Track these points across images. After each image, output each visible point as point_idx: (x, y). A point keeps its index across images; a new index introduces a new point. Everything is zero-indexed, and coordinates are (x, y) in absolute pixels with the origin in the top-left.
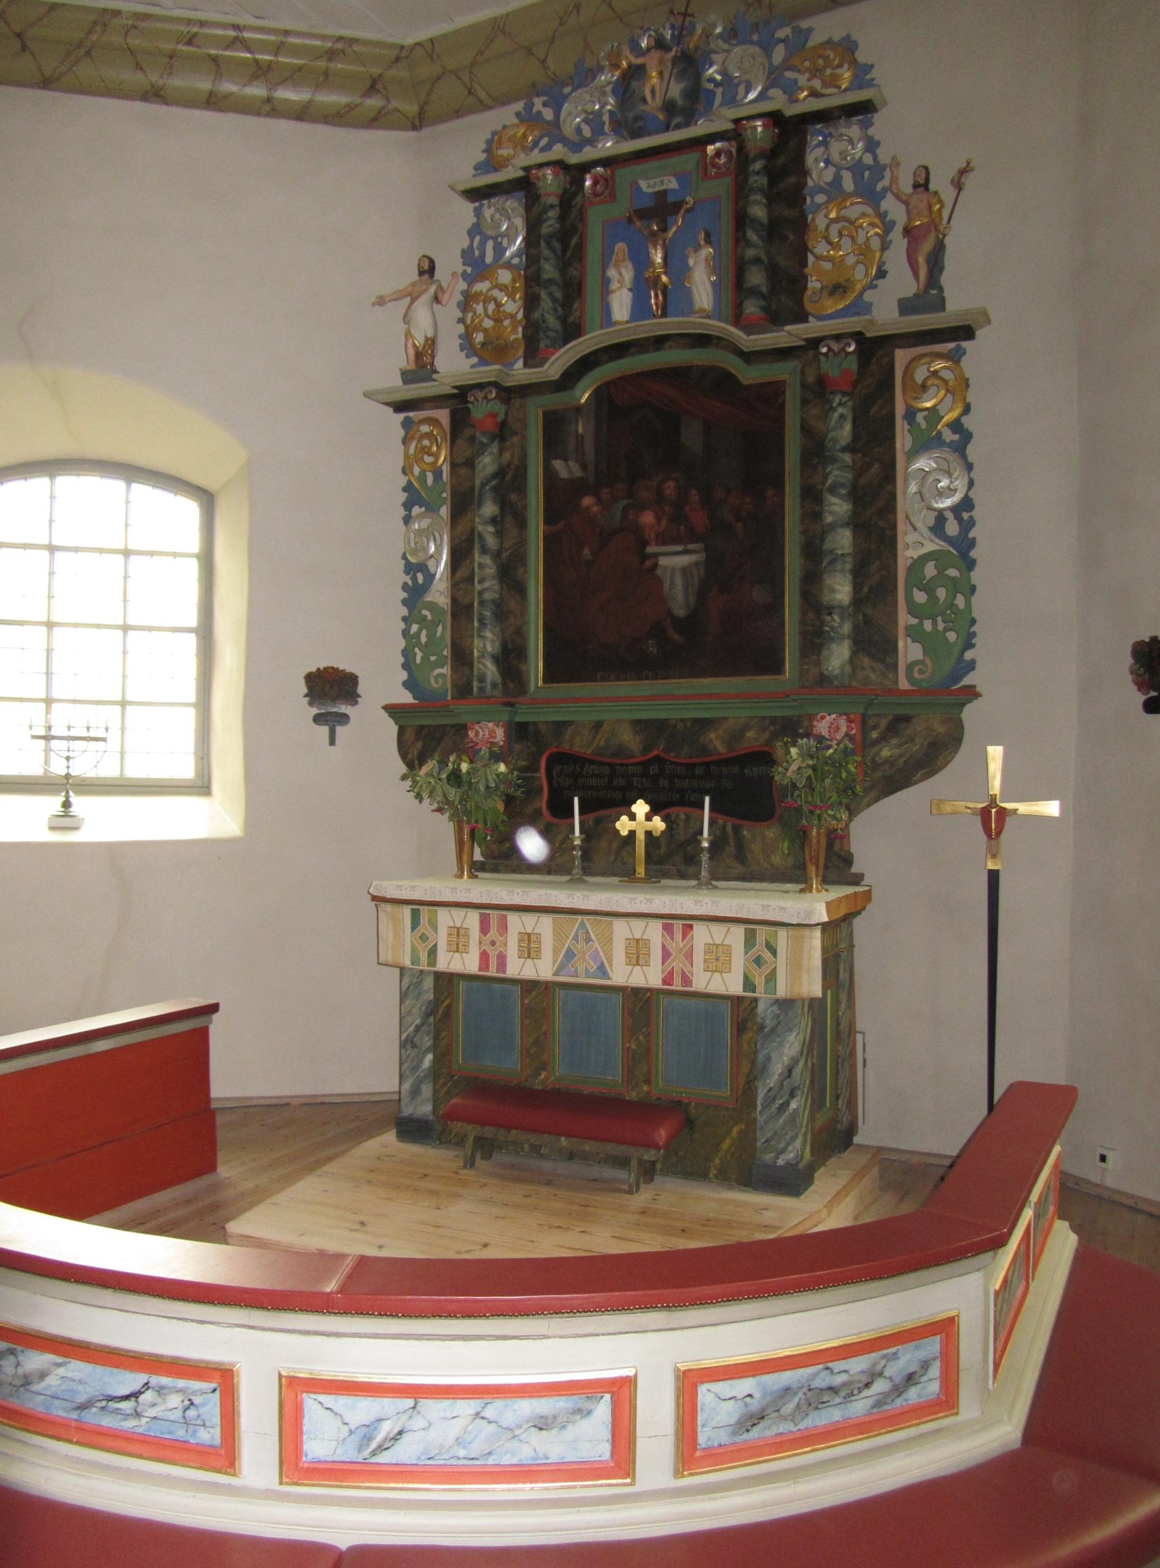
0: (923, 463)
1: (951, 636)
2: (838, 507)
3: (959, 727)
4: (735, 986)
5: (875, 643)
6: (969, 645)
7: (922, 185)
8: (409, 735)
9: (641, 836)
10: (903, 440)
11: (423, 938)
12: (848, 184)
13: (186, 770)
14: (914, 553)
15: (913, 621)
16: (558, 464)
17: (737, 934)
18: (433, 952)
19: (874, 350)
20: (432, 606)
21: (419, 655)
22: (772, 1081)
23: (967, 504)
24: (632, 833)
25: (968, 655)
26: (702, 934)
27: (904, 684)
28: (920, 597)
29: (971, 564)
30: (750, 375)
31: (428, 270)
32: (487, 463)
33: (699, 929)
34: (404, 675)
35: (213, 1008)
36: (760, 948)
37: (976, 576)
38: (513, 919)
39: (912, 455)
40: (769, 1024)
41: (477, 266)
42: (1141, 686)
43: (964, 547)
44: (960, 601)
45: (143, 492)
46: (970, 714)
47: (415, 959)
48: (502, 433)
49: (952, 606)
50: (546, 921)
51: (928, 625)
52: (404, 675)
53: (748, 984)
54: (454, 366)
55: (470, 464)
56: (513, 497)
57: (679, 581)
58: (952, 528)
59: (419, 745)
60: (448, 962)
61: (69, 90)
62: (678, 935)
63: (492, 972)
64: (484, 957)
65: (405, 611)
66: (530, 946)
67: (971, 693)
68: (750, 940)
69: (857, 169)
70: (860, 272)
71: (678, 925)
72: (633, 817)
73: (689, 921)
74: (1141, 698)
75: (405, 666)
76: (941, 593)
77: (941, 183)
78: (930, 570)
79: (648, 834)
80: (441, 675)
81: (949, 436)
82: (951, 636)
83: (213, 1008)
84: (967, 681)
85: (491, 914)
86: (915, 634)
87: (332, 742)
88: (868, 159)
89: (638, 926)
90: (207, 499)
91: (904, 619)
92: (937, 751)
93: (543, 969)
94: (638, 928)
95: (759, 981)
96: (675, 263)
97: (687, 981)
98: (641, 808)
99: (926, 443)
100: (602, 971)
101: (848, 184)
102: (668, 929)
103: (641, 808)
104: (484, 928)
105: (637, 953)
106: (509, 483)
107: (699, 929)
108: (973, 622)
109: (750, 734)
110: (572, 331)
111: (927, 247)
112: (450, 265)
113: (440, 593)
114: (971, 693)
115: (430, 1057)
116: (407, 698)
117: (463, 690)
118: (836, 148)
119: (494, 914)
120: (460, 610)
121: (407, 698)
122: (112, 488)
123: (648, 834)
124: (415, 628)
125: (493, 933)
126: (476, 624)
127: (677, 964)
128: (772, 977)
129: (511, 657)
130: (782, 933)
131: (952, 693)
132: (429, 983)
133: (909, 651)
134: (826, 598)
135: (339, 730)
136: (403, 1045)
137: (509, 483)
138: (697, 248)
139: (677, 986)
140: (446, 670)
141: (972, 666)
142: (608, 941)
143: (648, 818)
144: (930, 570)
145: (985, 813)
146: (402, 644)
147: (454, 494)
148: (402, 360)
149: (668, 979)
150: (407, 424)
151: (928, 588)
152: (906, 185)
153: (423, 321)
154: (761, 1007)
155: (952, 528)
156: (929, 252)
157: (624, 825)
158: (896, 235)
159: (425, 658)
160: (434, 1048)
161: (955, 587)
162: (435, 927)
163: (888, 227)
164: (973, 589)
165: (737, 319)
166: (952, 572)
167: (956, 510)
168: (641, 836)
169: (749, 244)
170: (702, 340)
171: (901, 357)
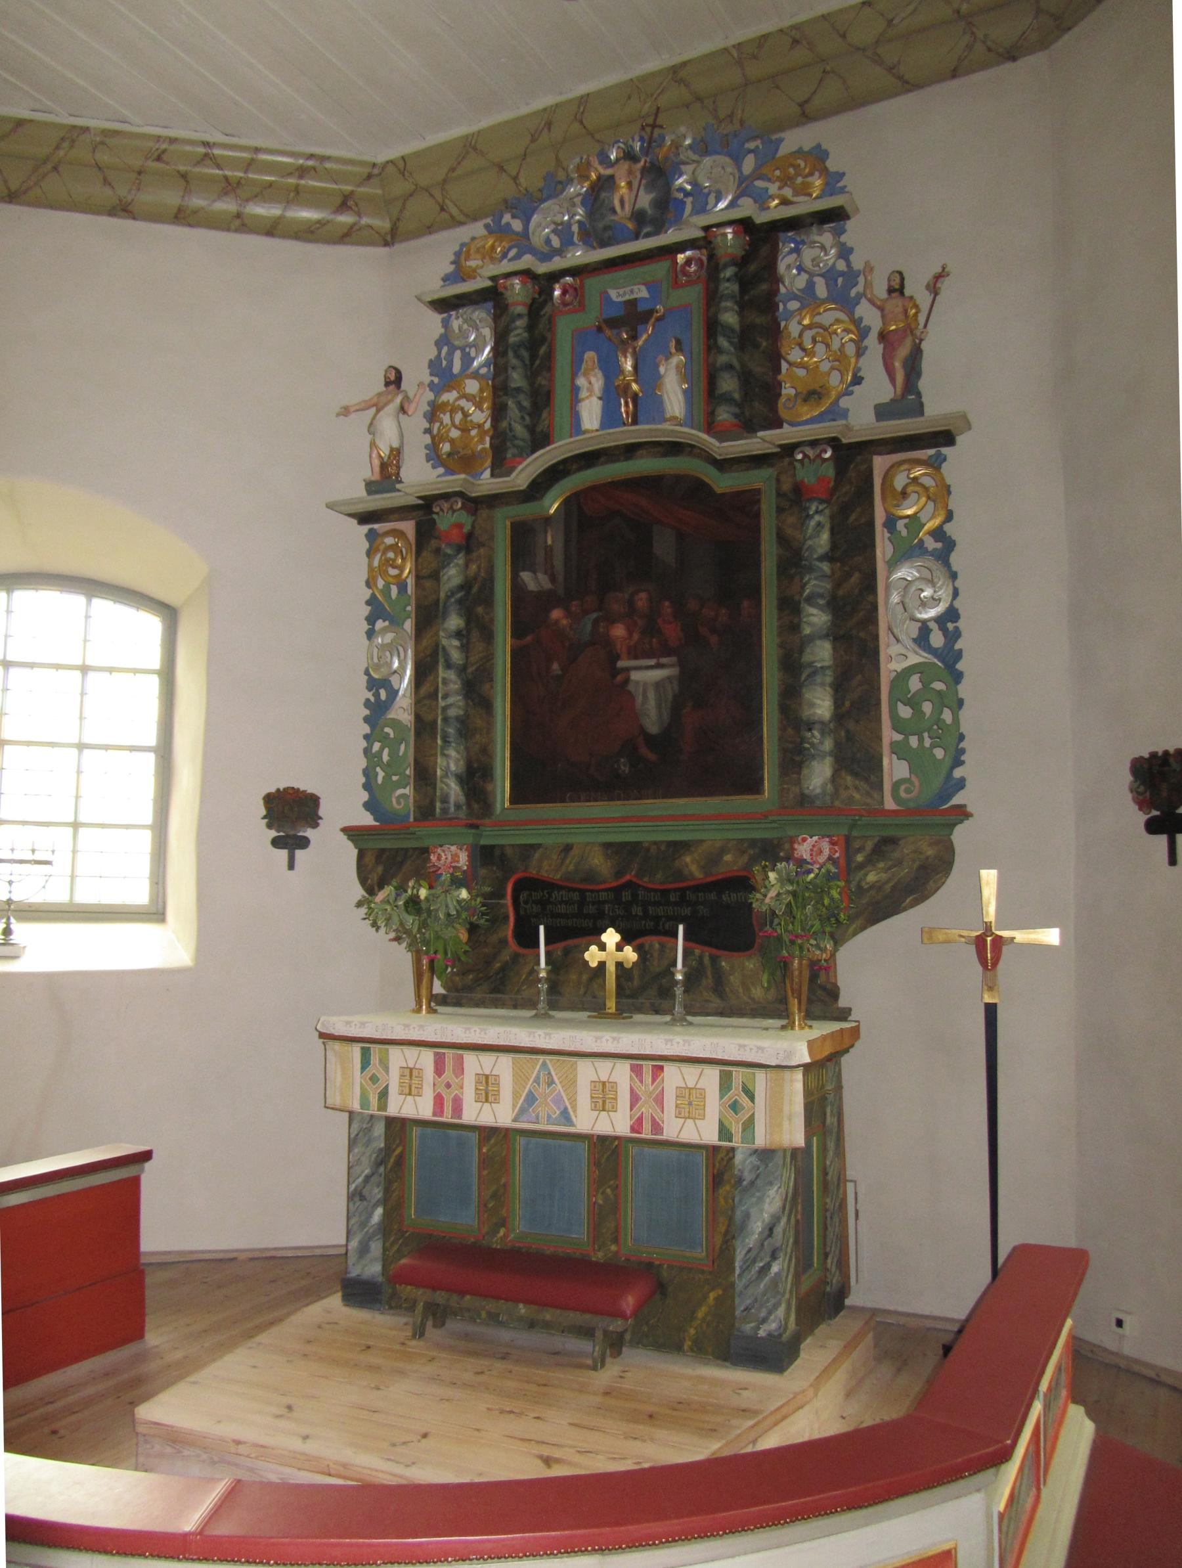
0: (906, 572)
1: (939, 753)
2: (816, 618)
3: (950, 849)
4: (708, 1134)
5: (857, 760)
6: (958, 762)
7: (897, 289)
8: (369, 859)
9: (611, 968)
10: (883, 548)
11: (374, 1079)
12: (821, 290)
13: (140, 895)
14: (898, 666)
15: (898, 737)
16: (526, 576)
17: (712, 1075)
18: (384, 1095)
19: (851, 456)
20: (395, 724)
21: (381, 774)
22: (752, 1240)
23: (951, 614)
24: (602, 965)
25: (958, 773)
26: (673, 1076)
27: (890, 804)
28: (905, 712)
29: (958, 677)
30: (723, 483)
31: (395, 380)
32: (453, 575)
33: (670, 1070)
34: (365, 796)
35: (145, 1156)
36: (736, 1092)
37: (963, 690)
38: (470, 1058)
39: (893, 564)
40: (748, 1177)
41: (443, 376)
42: (1142, 805)
43: (950, 658)
44: (947, 716)
45: (103, 607)
46: (960, 836)
47: (365, 1103)
48: (469, 544)
49: (939, 721)
50: (505, 1060)
51: (914, 741)
52: (365, 796)
53: (724, 1132)
54: (420, 476)
55: (435, 576)
56: (480, 610)
57: (651, 695)
58: (937, 639)
59: (380, 869)
60: (400, 1106)
61: (29, 204)
62: (648, 1077)
63: (447, 1118)
64: (439, 1101)
65: (367, 729)
66: (487, 1089)
67: (962, 813)
68: (725, 1083)
69: (830, 275)
70: (836, 380)
71: (647, 1066)
72: (602, 947)
73: (659, 1062)
74: (1142, 818)
75: (367, 786)
76: (927, 708)
77: (915, 287)
78: (915, 684)
79: (619, 965)
80: (403, 797)
81: (931, 544)
82: (939, 753)
83: (145, 1156)
84: (956, 800)
85: (446, 1053)
86: (900, 750)
87: (291, 866)
88: (841, 266)
89: (604, 1066)
90: (170, 614)
91: (889, 735)
92: (927, 875)
93: (501, 1114)
94: (604, 1068)
95: (736, 1129)
96: (646, 371)
97: (657, 1127)
98: (611, 937)
99: (908, 551)
100: (566, 1117)
101: (821, 290)
102: (637, 1071)
103: (611, 937)
104: (439, 1069)
105: (603, 1098)
106: (474, 597)
107: (670, 1070)
108: (962, 737)
109: (728, 858)
110: (540, 440)
111: (904, 351)
112: (417, 375)
113: (403, 711)
114: (962, 813)
115: (380, 1211)
116: (368, 820)
117: (425, 812)
118: (808, 254)
119: (449, 1053)
120: (424, 727)
121: (368, 820)
122: (72, 602)
123: (619, 965)
124: (376, 747)
125: (448, 1074)
126: (439, 742)
127: (646, 1109)
128: (749, 1124)
129: (476, 778)
130: (760, 1076)
131: (941, 813)
132: (379, 1130)
133: (895, 769)
134: (806, 713)
135: (299, 853)
136: (351, 1197)
137: (474, 597)
138: (668, 356)
139: (646, 1134)
140: (408, 790)
141: (961, 784)
142: (571, 1083)
143: (619, 948)
144: (915, 684)
145: (980, 942)
146: (363, 763)
147: (418, 607)
148: (367, 471)
149: (637, 1126)
150: (371, 536)
151: (913, 703)
152: (881, 291)
153: (388, 432)
154: (739, 1157)
155: (937, 639)
156: (907, 357)
157: (593, 956)
158: (872, 341)
159: (387, 777)
160: (385, 1201)
161: (941, 701)
162: (386, 1069)
163: (863, 333)
164: (961, 703)
165: (710, 427)
166: (939, 686)
167: (941, 620)
168: (611, 968)
169: (720, 351)
170: (674, 448)
171: (880, 463)
